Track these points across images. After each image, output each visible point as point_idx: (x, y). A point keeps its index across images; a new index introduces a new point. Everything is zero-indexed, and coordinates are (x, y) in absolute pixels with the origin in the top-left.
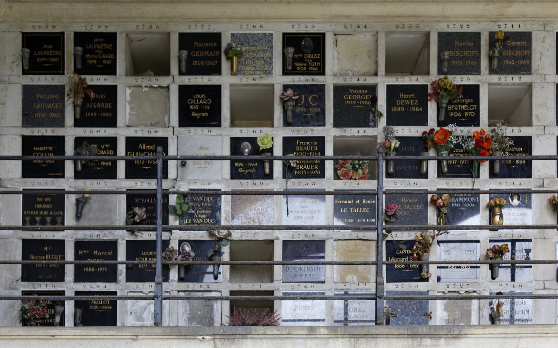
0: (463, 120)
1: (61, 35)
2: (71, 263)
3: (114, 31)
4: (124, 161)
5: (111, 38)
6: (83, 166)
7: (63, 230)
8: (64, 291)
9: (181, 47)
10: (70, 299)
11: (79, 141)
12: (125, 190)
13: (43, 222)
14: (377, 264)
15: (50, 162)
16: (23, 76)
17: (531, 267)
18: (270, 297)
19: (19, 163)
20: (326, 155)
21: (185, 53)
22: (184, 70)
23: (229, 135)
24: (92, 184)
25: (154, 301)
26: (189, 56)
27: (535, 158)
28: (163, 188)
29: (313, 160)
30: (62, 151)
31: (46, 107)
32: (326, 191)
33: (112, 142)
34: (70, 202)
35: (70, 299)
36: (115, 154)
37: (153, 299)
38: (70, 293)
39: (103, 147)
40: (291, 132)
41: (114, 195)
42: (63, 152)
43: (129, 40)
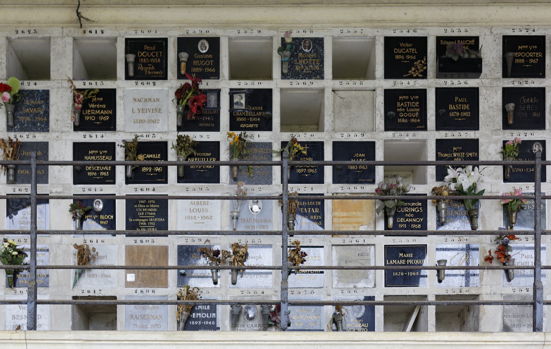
0: (98, 123)
1: (129, 42)
3: (543, 34)
4: (434, 167)
5: (319, 43)
6: (133, 171)
7: (167, 236)
8: (374, 297)
9: (127, 51)
10: (380, 304)
12: (6, 195)
13: (409, 226)
14: (535, 269)
15: (363, 167)
16: (126, 81)
17: (322, 272)
18: (113, 301)
19: (70, 168)
20: (49, 160)
21: (131, 58)
22: (131, 74)
23: (71, 140)
24: (527, 187)
25: (26, 305)
26: (137, 60)
27: (327, 163)
28: (38, 193)
29: (196, 165)
30: (217, 155)
31: (31, 111)
32: (546, 195)
33: (110, 147)
34: (121, 207)
35: (380, 304)
36: (114, 159)
37: (27, 304)
38: (379, 298)
39: (101, 153)
40: (443, 135)
41: (174, 200)
42: (373, 158)
43: (334, 44)
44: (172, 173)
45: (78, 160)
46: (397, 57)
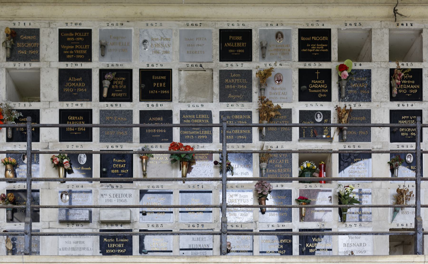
11: (143, 114)
20: (93, 123)
30: (170, 121)
45: (394, 123)
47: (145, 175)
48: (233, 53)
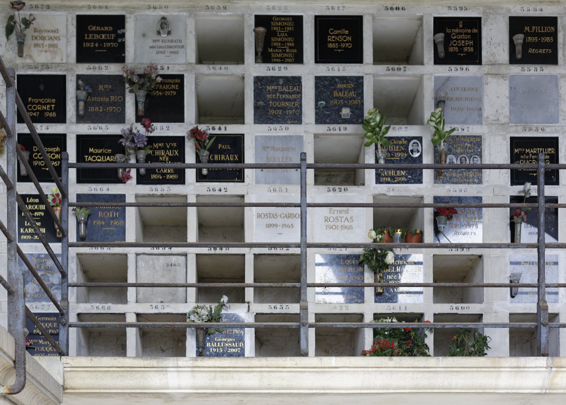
2: (249, 286)
44: (191, 174)
46: (330, 46)
47: (513, 240)
48: (335, 48)
